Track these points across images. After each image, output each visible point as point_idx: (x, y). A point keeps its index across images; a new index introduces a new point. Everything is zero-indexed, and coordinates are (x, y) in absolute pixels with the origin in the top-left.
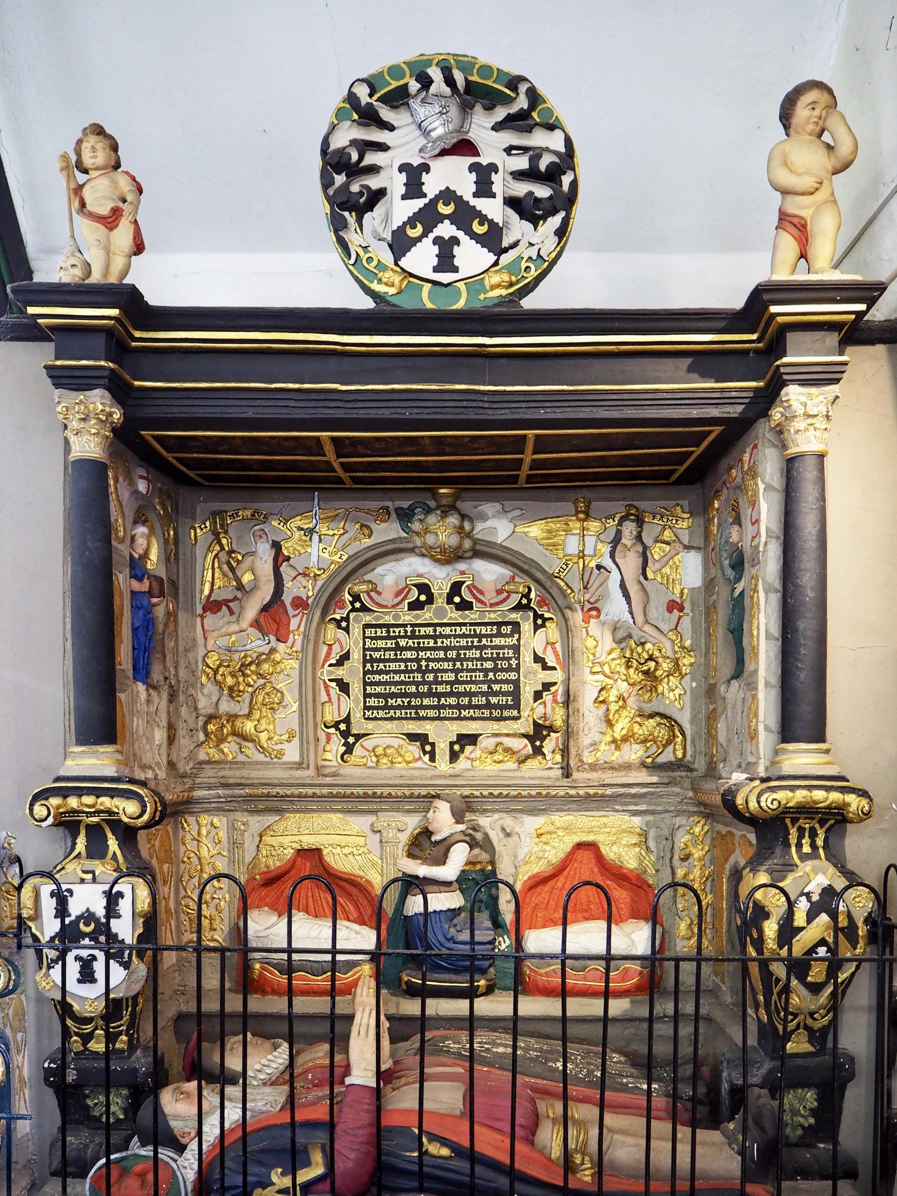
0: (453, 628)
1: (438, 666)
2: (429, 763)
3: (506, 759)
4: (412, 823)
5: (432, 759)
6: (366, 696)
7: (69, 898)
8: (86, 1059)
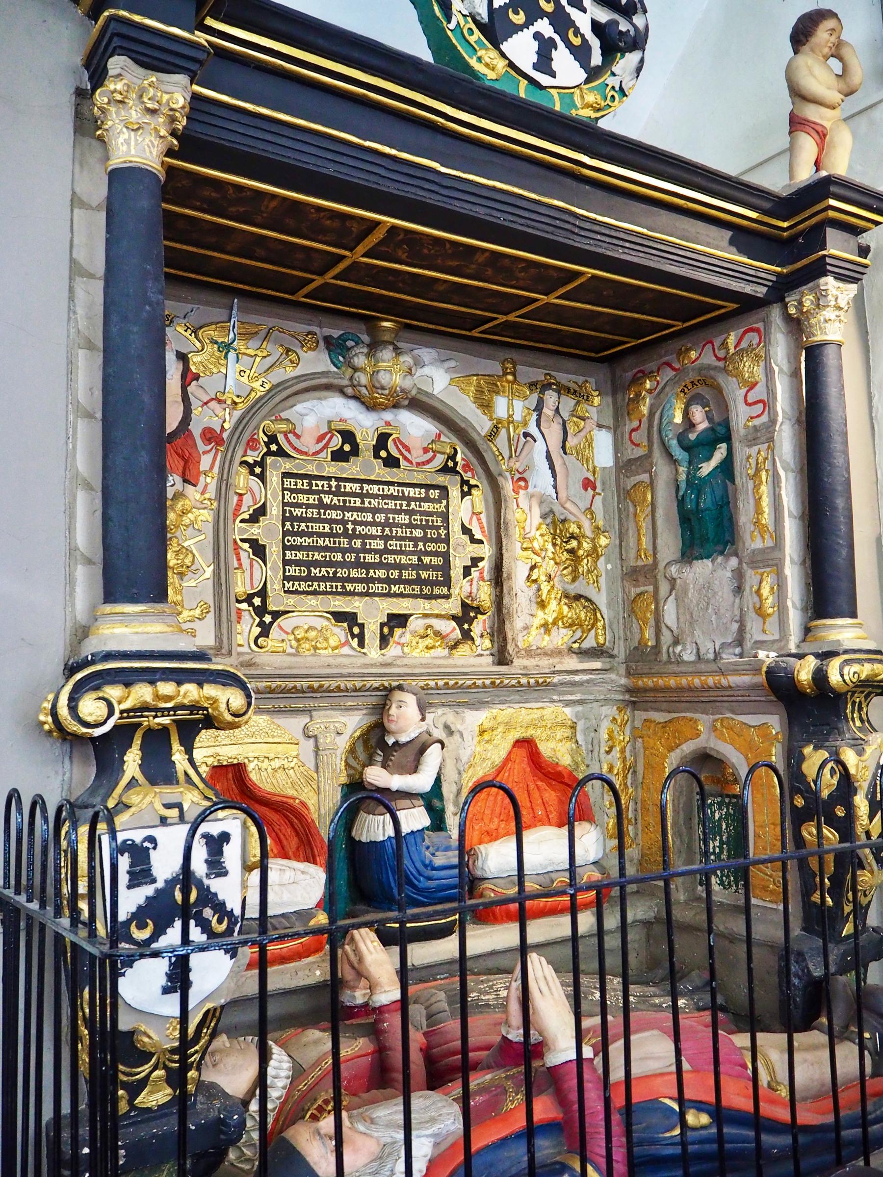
0: (381, 487)
1: (366, 530)
2: (359, 649)
3: (437, 644)
4: (353, 722)
5: (361, 644)
6: (286, 563)
7: (151, 851)
8: (134, 1124)
